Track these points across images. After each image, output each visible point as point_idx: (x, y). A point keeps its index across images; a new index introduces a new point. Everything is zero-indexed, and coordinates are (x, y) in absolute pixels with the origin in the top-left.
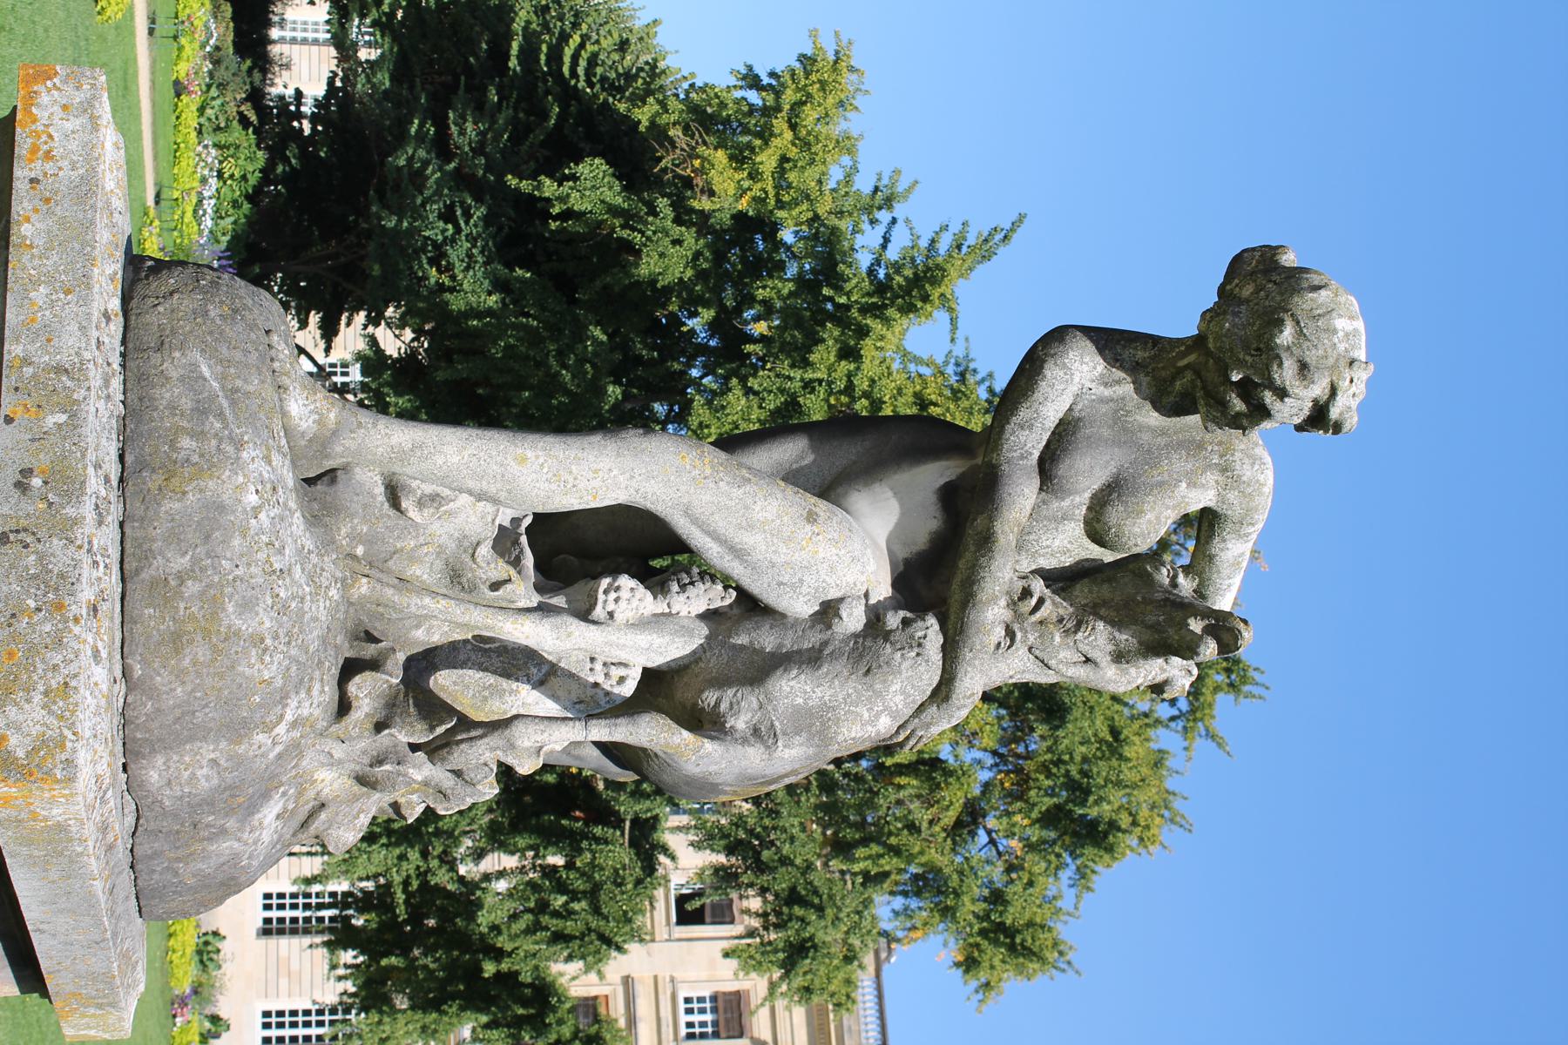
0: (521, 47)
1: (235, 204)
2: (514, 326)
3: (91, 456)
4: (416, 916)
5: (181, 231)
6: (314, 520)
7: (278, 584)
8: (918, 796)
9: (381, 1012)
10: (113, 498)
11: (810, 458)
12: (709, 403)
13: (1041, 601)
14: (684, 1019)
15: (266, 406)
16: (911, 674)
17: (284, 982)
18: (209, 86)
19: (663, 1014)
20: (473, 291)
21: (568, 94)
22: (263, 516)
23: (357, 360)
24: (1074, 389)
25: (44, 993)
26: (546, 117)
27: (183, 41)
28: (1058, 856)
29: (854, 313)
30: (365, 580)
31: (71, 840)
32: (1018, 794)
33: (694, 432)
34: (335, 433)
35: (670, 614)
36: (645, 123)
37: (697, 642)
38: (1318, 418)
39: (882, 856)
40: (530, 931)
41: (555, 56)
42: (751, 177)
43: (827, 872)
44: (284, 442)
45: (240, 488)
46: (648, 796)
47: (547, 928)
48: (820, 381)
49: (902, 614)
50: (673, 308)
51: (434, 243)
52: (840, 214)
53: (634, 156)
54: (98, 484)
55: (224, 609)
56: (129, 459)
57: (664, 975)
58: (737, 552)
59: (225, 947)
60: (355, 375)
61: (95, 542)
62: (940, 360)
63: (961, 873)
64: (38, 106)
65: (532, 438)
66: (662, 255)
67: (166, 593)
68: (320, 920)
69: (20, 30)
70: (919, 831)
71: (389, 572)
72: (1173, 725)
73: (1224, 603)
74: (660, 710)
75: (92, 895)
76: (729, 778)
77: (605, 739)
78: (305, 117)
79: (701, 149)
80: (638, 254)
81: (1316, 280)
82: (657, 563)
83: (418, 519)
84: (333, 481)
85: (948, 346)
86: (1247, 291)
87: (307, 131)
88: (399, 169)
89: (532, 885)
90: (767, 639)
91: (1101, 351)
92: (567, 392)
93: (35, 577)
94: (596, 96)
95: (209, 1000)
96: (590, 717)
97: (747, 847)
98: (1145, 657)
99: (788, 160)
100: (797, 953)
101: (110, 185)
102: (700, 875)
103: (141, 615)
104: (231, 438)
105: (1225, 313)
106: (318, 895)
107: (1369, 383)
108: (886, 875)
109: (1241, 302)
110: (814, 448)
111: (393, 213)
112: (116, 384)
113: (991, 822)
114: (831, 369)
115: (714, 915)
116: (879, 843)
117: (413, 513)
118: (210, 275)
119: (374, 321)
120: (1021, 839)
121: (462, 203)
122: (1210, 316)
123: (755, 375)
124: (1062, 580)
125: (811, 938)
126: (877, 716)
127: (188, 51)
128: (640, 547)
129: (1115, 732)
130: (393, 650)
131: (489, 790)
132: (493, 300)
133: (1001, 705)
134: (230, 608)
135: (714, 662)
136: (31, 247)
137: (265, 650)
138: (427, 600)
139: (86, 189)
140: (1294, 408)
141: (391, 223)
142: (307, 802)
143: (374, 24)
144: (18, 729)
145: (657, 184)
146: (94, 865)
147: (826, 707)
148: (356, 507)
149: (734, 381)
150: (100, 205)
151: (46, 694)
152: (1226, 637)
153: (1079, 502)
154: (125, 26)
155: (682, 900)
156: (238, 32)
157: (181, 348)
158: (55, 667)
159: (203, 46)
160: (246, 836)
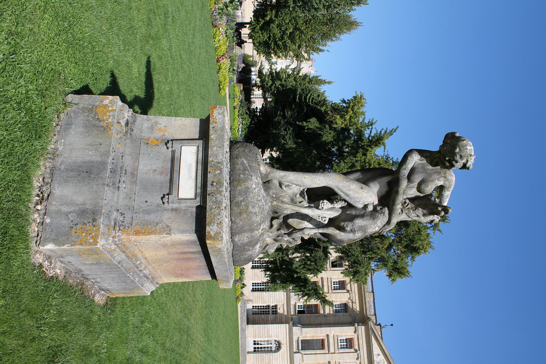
1: (245, 129)
3: (224, 179)
4: (281, 265)
6: (265, 190)
12: (337, 165)
13: (408, 204)
16: (382, 220)
20: (290, 144)
21: (308, 106)
25: (216, 279)
29: (365, 147)
32: (400, 242)
38: (464, 167)
40: (303, 268)
41: (305, 98)
43: (362, 257)
45: (252, 184)
52: (362, 127)
53: (321, 117)
54: (226, 184)
57: (329, 277)
58: (347, 195)
60: (268, 161)
67: (238, 204)
73: (445, 204)
74: (333, 226)
81: (463, 139)
86: (449, 142)
90: (354, 212)
91: (419, 154)
92: (309, 164)
95: (242, 281)
96: (319, 228)
97: (346, 252)
101: (227, 127)
102: (336, 258)
108: (373, 258)
109: (448, 143)
110: (362, 174)
112: (229, 165)
113: (394, 247)
114: (361, 158)
117: (284, 188)
119: (271, 150)
124: (412, 200)
128: (329, 194)
129: (419, 229)
131: (299, 242)
135: (343, 217)
139: (223, 128)
145: (326, 122)
146: (226, 256)
153: (415, 184)
154: (225, 97)
155: (332, 263)
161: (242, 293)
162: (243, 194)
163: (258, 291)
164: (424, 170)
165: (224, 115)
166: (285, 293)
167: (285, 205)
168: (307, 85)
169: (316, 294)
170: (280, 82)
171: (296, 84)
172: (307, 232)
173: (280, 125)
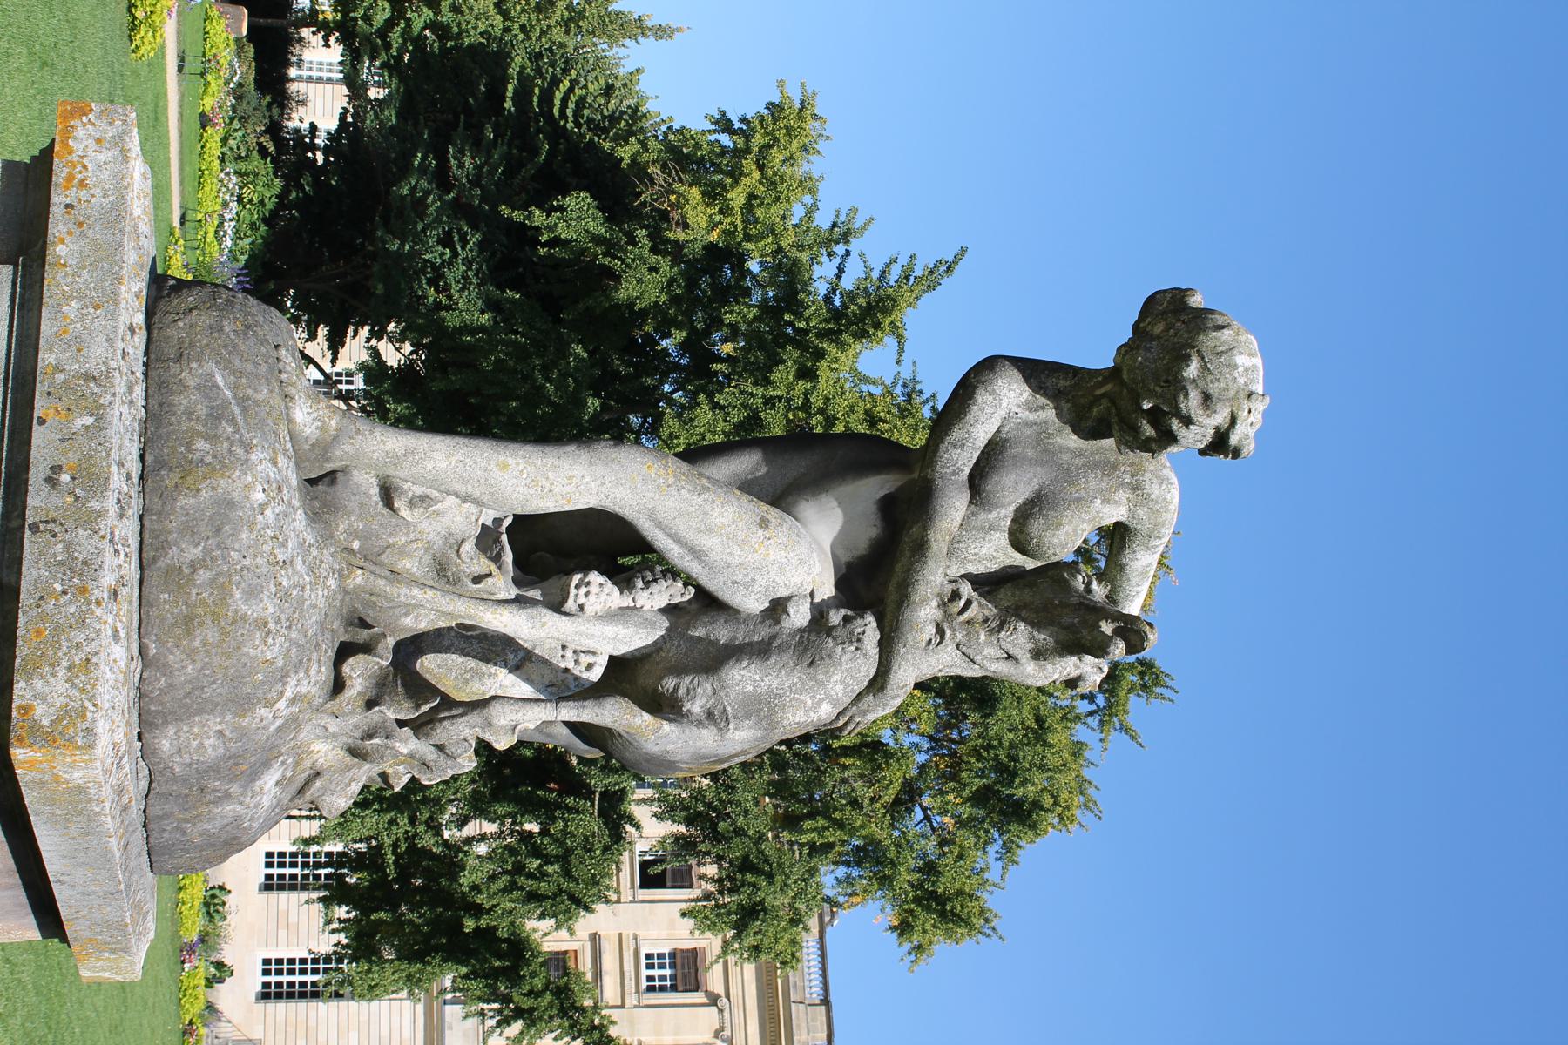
0: (515, 90)
1: (253, 226)
2: (503, 343)
3: (115, 455)
4: (404, 875)
5: (203, 250)
6: (314, 517)
7: (280, 573)
8: (862, 776)
9: (371, 962)
10: (133, 493)
11: (763, 470)
12: (679, 416)
13: (968, 603)
14: (645, 973)
15: (274, 414)
16: (849, 668)
17: (283, 933)
18: (232, 119)
19: (626, 969)
21: (557, 133)
22: (268, 512)
23: (360, 370)
24: (1002, 413)
25: (64, 939)
26: (537, 153)
27: (209, 77)
28: (987, 831)
29: (812, 337)
30: (359, 572)
31: (90, 801)
33: (665, 442)
34: (335, 438)
35: (635, 608)
36: (627, 161)
37: (659, 633)
38: (1220, 444)
39: (827, 828)
40: (506, 890)
41: (547, 97)
42: (721, 211)
43: (775, 843)
44: (289, 446)
46: (616, 771)
47: (522, 888)
48: (780, 399)
49: (843, 611)
50: (649, 329)
51: (433, 265)
53: (617, 192)
55: (232, 596)
56: (149, 458)
57: (628, 933)
58: (697, 554)
59: (228, 899)
60: (359, 383)
61: (117, 533)
62: (888, 382)
63: (898, 845)
64: (74, 138)
65: (513, 446)
66: (639, 281)
67: (178, 578)
68: (317, 877)
69: (61, 66)
70: (861, 807)
71: (382, 565)
72: (1090, 720)
73: (1133, 608)
74: (624, 694)
75: (107, 850)
76: (685, 757)
77: (573, 719)
78: (319, 149)
79: (677, 186)
80: (618, 279)
81: (1220, 320)
82: (627, 561)
83: (409, 518)
84: (333, 482)
85: (894, 369)
86: (1158, 329)
87: (320, 161)
88: (403, 198)
89: (510, 849)
90: (722, 633)
91: (1027, 379)
92: (551, 403)
93: (62, 563)
94: (582, 136)
95: (214, 949)
96: (561, 699)
97: (705, 817)
98: (1061, 655)
99: (756, 197)
100: (748, 915)
101: (137, 211)
102: (662, 842)
103: (158, 599)
104: (241, 442)
105: (1138, 348)
106: (315, 855)
107: (1265, 414)
108: (831, 846)
109: (1152, 338)
110: (767, 460)
111: (395, 237)
112: (139, 390)
113: (927, 801)
114: (789, 388)
115: (674, 880)
116: (826, 818)
117: (404, 512)
118: (225, 294)
119: (377, 334)
120: (952, 817)
121: (459, 230)
122: (1125, 350)
123: (721, 392)
124: (987, 584)
125: (762, 902)
126: (820, 703)
127: (213, 86)
128: (601, 546)
129: (1040, 721)
130: (384, 635)
131: (468, 763)
132: (485, 319)
133: (938, 695)
134: (238, 595)
136: (65, 265)
137: (268, 634)
138: (416, 591)
139: (116, 215)
140: (1197, 435)
141: (394, 246)
142: (304, 771)
143: (383, 66)
144: (44, 700)
145: (637, 216)
146: (110, 824)
147: (774, 695)
148: (353, 506)
149: (702, 397)
150: (128, 229)
151: (70, 668)
152: (1134, 638)
153: (1004, 515)
154: (157, 63)
155: (645, 865)
156: (259, 70)
157: (199, 359)
158: (78, 645)
159: (227, 83)
160: (247, 800)
161: (210, 1007)
162: (204, 530)
163: (290, 996)
164: (1046, 452)
165: (124, 153)
166: (420, 1007)
167: (405, 591)
168: (557, 35)
169: (563, 1012)
170: (428, 14)
171: (507, 30)
172: (503, 716)
173: (422, 217)
